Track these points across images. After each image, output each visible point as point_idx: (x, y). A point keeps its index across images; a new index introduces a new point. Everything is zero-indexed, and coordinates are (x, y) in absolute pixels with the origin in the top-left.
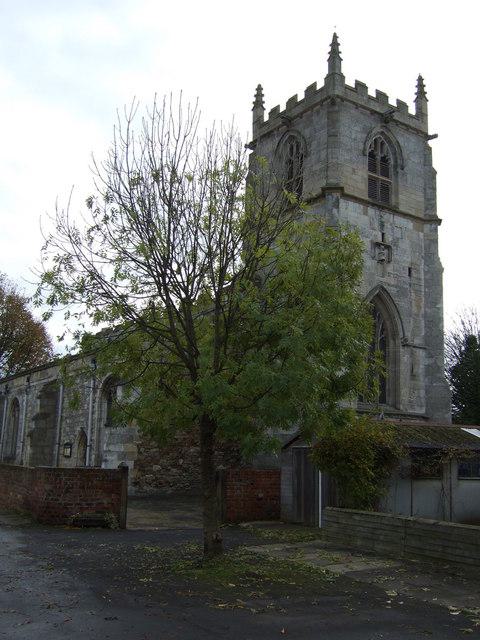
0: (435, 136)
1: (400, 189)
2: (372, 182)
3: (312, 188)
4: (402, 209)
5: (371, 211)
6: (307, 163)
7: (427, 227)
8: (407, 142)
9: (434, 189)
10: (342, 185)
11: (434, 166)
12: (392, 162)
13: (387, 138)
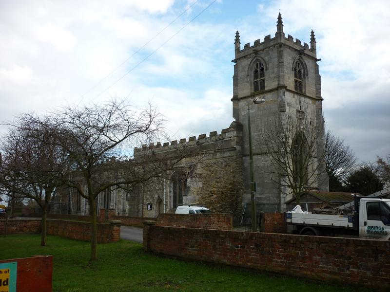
0: (320, 60)
1: (306, 85)
2: (296, 81)
3: (270, 85)
4: (307, 94)
5: (296, 96)
6: (267, 73)
7: (317, 103)
8: (309, 63)
9: (320, 85)
10: (286, 85)
11: (320, 74)
12: (303, 72)
13: (301, 61)
